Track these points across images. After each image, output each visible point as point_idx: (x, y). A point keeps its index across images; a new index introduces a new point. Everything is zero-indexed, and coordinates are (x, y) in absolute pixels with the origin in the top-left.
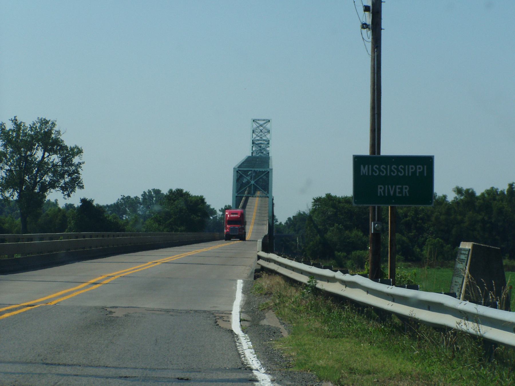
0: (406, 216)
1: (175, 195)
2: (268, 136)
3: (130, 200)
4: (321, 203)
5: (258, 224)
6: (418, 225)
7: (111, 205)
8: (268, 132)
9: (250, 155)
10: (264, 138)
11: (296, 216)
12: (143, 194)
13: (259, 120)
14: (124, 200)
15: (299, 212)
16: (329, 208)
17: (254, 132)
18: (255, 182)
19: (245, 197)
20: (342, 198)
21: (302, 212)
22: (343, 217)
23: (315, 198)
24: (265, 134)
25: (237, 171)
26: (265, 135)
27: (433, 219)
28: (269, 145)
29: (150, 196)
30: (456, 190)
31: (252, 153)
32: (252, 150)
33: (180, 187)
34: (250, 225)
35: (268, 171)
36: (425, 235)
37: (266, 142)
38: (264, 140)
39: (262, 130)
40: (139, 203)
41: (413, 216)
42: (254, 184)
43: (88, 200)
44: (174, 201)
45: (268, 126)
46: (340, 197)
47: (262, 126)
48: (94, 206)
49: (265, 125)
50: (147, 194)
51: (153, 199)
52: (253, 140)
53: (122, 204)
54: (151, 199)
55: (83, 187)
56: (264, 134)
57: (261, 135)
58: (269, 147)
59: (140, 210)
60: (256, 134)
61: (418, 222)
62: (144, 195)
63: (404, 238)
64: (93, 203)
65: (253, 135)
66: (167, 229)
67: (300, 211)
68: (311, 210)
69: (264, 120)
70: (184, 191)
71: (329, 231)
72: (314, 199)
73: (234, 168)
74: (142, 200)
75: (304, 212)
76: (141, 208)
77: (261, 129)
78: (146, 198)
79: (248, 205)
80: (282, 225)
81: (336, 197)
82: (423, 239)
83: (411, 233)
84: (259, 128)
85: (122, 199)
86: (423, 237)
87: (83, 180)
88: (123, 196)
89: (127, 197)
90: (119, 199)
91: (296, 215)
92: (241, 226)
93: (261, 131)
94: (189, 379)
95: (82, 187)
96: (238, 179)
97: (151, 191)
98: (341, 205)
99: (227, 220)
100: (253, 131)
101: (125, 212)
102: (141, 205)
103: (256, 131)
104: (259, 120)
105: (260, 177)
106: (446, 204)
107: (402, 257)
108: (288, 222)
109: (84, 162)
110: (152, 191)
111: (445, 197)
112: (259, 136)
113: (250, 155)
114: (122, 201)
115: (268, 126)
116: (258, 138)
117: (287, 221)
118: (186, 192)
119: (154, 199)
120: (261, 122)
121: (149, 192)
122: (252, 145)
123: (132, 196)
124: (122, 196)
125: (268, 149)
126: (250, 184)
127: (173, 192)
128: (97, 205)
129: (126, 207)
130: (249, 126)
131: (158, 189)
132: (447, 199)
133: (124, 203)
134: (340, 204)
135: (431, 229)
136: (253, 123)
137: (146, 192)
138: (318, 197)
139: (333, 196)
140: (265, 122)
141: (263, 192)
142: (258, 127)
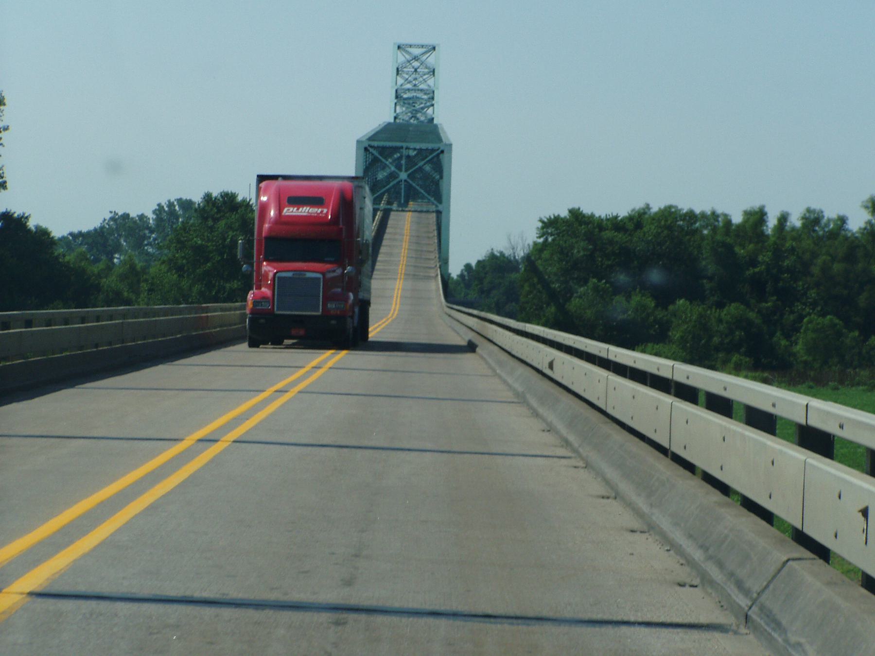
0: (753, 263)
1: (217, 208)
2: (431, 82)
3: (128, 221)
4: (557, 229)
5: (415, 277)
6: (781, 284)
7: (89, 233)
8: (432, 73)
9: (392, 120)
10: (422, 86)
11: (484, 261)
12: (156, 210)
13: (411, 46)
14: (116, 223)
15: (490, 251)
16: (576, 242)
17: (400, 72)
18: (409, 176)
19: (382, 212)
20: (607, 220)
21: (498, 252)
22: (610, 263)
23: (545, 217)
24: (425, 77)
25: (366, 149)
26: (424, 80)
27: (816, 270)
28: (433, 102)
29: (172, 213)
30: (870, 205)
31: (395, 118)
32: (395, 111)
33: (230, 188)
34: (395, 279)
35: (442, 148)
36: (798, 306)
37: (425, 94)
38: (422, 90)
39: (418, 68)
40: (148, 228)
41: (769, 262)
42: (405, 181)
43: (16, 215)
44: (216, 220)
45: (431, 59)
46: (603, 216)
47: (417, 60)
48: (30, 231)
49: (425, 57)
50: (166, 209)
51: (177, 219)
52: (396, 91)
53: (111, 231)
54: (175, 221)
55: (6, 186)
56: (422, 77)
57: (415, 79)
58: (433, 105)
59: (149, 244)
60: (402, 77)
61: (782, 276)
62: (159, 211)
63: (752, 315)
64: (28, 224)
65: (396, 79)
66: (200, 286)
67: (492, 249)
68: (531, 247)
69: (423, 46)
70: (240, 198)
71: (575, 295)
72: (543, 222)
73: (359, 142)
74: (155, 222)
75: (501, 253)
76: (152, 239)
77: (415, 67)
78: (162, 218)
79: (388, 233)
80: (453, 278)
81: (592, 215)
82: (792, 317)
83: (767, 302)
84: (411, 64)
85: (112, 219)
86: (792, 312)
87: (4, 168)
88: (115, 212)
89: (121, 216)
90: (105, 220)
91: (484, 258)
92: (339, 271)
93: (416, 70)
94: (414, 73)
95: (3, 186)
96: (366, 167)
97: (173, 203)
98: (607, 234)
99: (264, 234)
100: (398, 69)
101: (118, 248)
102: (152, 232)
103: (405, 70)
104: (411, 46)
105: (417, 167)
106: (846, 238)
107: (748, 359)
108: (466, 273)
109: (8, 126)
110: (175, 203)
111: (843, 220)
112: (410, 82)
113: (392, 120)
114: (112, 223)
115: (431, 59)
116: (409, 86)
117: (462, 271)
118: (244, 201)
119: (180, 220)
120: (416, 51)
121: (171, 205)
122: (395, 101)
123: (133, 214)
124: (111, 212)
125: (430, 111)
126: (397, 180)
127: (213, 199)
128: (37, 227)
129: (120, 236)
130: (390, 59)
131: (188, 199)
132: (847, 227)
133: (117, 228)
134: (603, 233)
135: (813, 294)
136: (399, 52)
137: (163, 204)
138: (552, 217)
139: (586, 215)
140: (424, 50)
141: (429, 200)
142: (409, 61)
